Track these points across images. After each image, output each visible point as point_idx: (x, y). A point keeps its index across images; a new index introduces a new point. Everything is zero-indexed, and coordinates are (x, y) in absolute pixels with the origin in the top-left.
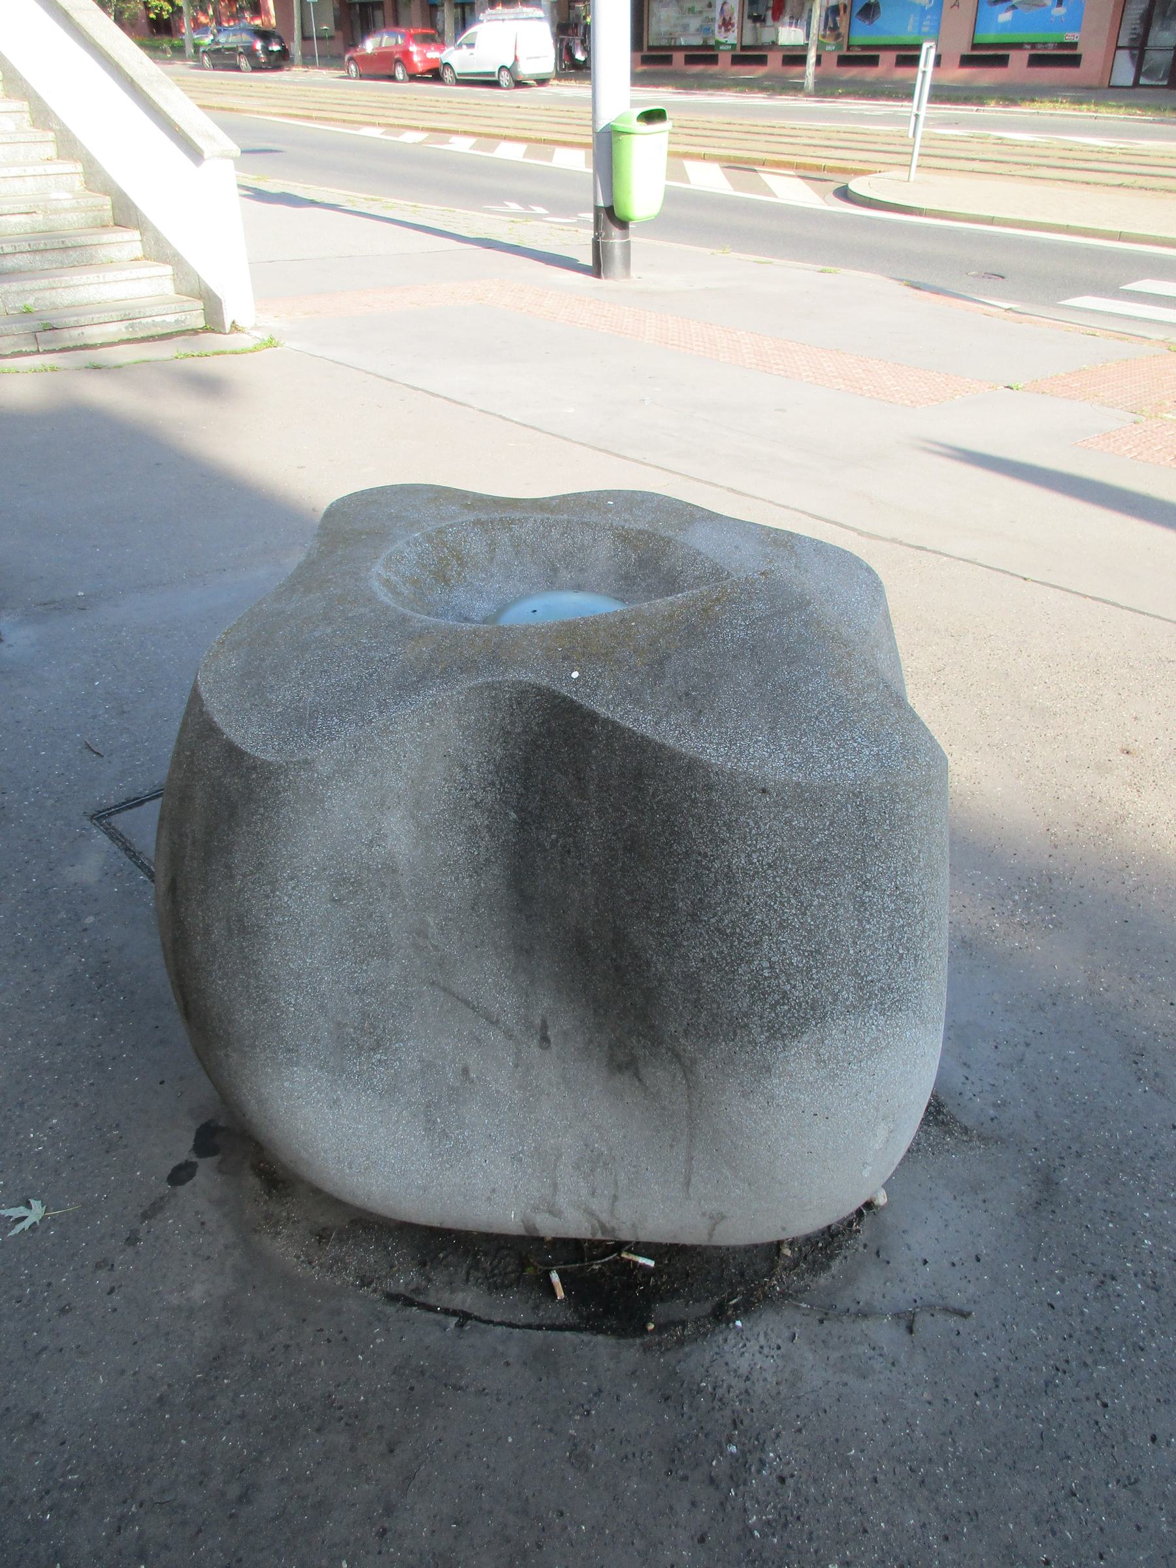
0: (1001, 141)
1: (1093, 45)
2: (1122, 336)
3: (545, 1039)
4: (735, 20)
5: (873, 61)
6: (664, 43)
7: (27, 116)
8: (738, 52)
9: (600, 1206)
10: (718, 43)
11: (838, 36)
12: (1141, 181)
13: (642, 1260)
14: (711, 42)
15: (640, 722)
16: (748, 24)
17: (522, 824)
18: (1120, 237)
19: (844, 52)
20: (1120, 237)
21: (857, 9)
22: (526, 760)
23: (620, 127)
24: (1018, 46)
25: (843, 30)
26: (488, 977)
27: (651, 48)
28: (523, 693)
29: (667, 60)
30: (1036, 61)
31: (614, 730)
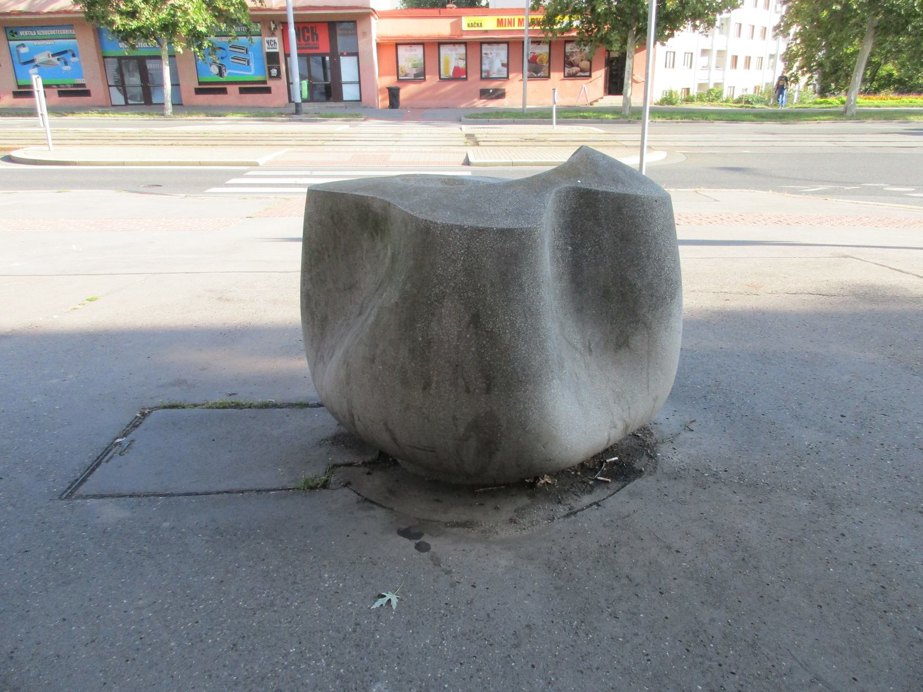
1: (95, 83)
2: (258, 198)
3: (591, 351)
12: (184, 142)
13: (613, 459)
17: (575, 251)
18: (200, 164)
22: (571, 221)
28: (568, 191)
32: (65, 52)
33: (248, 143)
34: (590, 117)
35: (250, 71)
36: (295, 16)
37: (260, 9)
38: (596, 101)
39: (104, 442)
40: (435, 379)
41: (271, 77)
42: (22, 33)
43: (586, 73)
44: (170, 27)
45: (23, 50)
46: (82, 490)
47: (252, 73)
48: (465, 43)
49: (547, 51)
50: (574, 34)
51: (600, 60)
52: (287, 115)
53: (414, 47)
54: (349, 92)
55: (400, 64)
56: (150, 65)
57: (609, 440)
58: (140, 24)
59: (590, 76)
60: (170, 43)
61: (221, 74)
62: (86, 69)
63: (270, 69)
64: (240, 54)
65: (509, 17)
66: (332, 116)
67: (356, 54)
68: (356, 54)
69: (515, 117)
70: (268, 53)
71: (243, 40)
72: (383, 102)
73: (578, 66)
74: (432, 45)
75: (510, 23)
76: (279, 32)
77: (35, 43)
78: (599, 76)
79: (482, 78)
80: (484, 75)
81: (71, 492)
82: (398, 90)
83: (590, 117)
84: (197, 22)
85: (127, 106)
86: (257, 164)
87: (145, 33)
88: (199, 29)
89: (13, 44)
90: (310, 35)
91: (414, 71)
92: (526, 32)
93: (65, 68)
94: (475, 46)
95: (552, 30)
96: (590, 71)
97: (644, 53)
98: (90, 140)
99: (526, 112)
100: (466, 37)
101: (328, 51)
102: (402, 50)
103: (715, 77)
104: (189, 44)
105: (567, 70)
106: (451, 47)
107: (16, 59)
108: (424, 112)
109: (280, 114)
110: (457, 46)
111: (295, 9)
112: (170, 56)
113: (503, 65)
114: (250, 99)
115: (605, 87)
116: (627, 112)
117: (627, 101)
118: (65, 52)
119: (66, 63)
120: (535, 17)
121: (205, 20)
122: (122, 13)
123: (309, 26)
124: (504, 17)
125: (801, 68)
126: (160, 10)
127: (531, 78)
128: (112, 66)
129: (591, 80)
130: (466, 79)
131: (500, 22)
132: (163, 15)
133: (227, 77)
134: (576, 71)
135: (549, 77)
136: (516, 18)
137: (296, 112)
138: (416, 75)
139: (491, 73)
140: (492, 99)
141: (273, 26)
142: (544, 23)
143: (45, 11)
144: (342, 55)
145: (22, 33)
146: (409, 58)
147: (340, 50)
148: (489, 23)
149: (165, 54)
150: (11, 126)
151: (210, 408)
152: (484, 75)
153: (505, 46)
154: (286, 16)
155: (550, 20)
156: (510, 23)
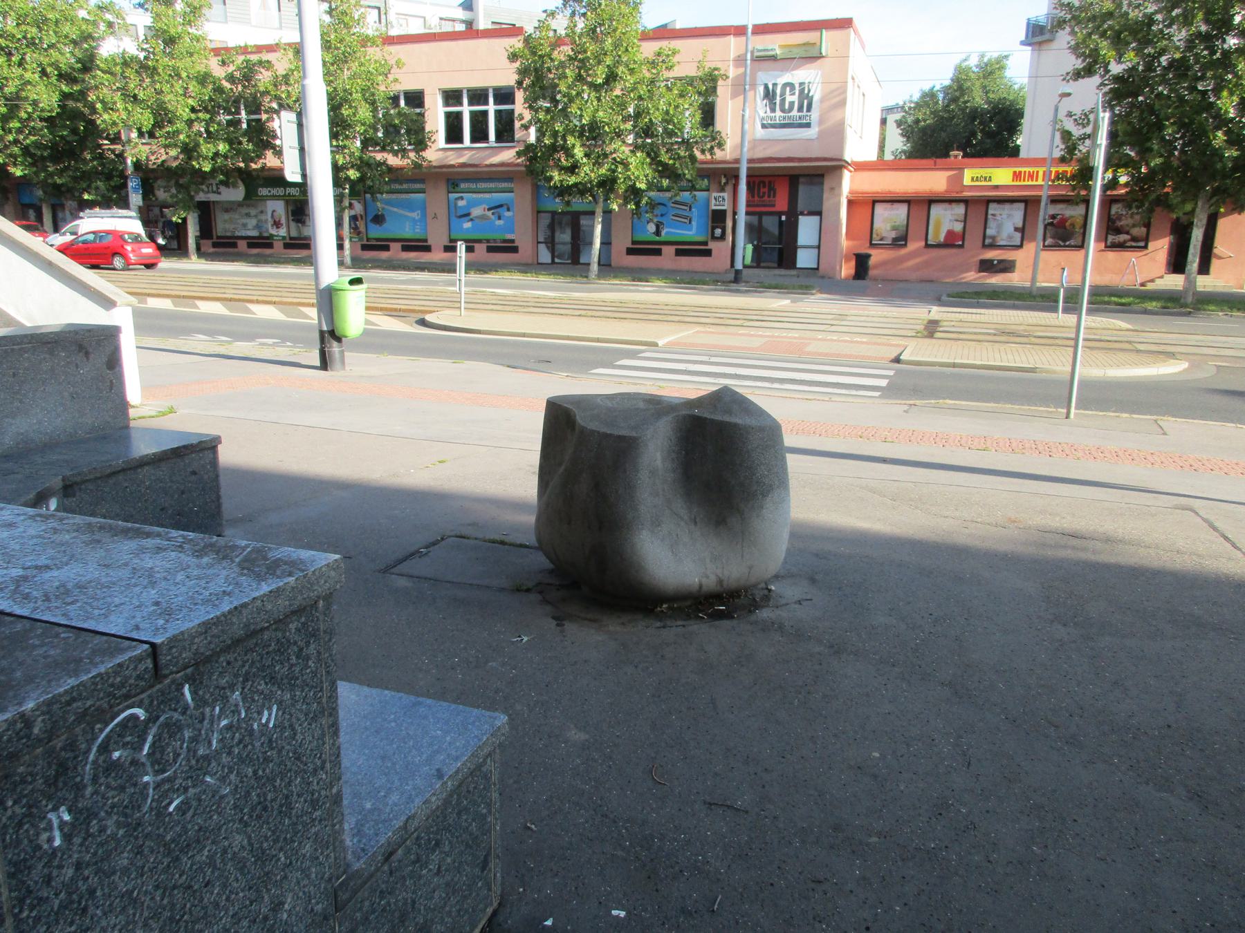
0: (495, 294)
1: (523, 236)
4: (283, 221)
5: (387, 248)
6: (229, 234)
7: (1028, 284)
8: (288, 241)
9: (719, 572)
10: (272, 236)
11: (359, 233)
12: (594, 313)
14: (266, 235)
15: (718, 417)
16: (293, 225)
18: (598, 340)
19: (365, 242)
20: (598, 340)
21: (370, 218)
23: (338, 286)
24: (479, 241)
25: (362, 229)
26: (680, 505)
27: (218, 237)
28: (684, 417)
29: (234, 245)
30: (491, 249)
31: (712, 421)
32: (501, 206)
33: (660, 317)
35: (690, 230)
36: (748, 169)
37: (712, 162)
38: (1152, 281)
39: (413, 549)
41: (714, 238)
42: (462, 186)
43: (1141, 243)
44: (608, 184)
45: (461, 203)
46: (395, 570)
47: (692, 232)
48: (966, 202)
52: (723, 282)
53: (896, 205)
54: (804, 259)
55: (875, 226)
56: (584, 221)
57: (701, 586)
58: (579, 180)
59: (1146, 247)
60: (606, 199)
61: (658, 233)
62: (519, 224)
63: (713, 228)
64: (684, 211)
65: (1031, 170)
66: (770, 287)
67: (819, 213)
68: (819, 213)
69: (1018, 299)
70: (714, 211)
71: (686, 195)
72: (846, 270)
73: (1127, 233)
74: (921, 204)
75: (1031, 176)
76: (729, 188)
77: (474, 196)
78: (1161, 247)
79: (927, 246)
80: (987, 241)
81: (386, 570)
82: (868, 256)
84: (638, 178)
85: (550, 268)
86: (656, 345)
87: (581, 189)
88: (638, 185)
89: (453, 196)
90: (766, 190)
91: (893, 235)
92: (1046, 188)
93: (501, 222)
94: (979, 205)
97: (1083, 252)
98: (504, 305)
100: (966, 194)
101: (785, 208)
102: (879, 209)
104: (626, 202)
105: (1110, 238)
106: (946, 205)
107: (452, 210)
108: (896, 289)
109: (716, 282)
110: (954, 205)
111: (750, 161)
112: (604, 212)
113: (1016, 229)
114: (686, 262)
116: (1190, 300)
118: (501, 206)
119: (499, 218)
121: (646, 176)
122: (561, 169)
123: (767, 180)
124: (1023, 170)
126: (600, 165)
127: (1046, 247)
128: (545, 220)
129: (1145, 252)
130: (962, 246)
131: (1017, 176)
132: (603, 171)
133: (663, 238)
137: (734, 280)
138: (895, 240)
141: (723, 181)
142: (1073, 177)
143: (488, 162)
144: (802, 214)
145: (462, 186)
146: (888, 219)
147: (800, 207)
149: (599, 211)
150: (435, 283)
152: (987, 241)
153: (1022, 206)
154: (738, 169)
156: (1031, 176)
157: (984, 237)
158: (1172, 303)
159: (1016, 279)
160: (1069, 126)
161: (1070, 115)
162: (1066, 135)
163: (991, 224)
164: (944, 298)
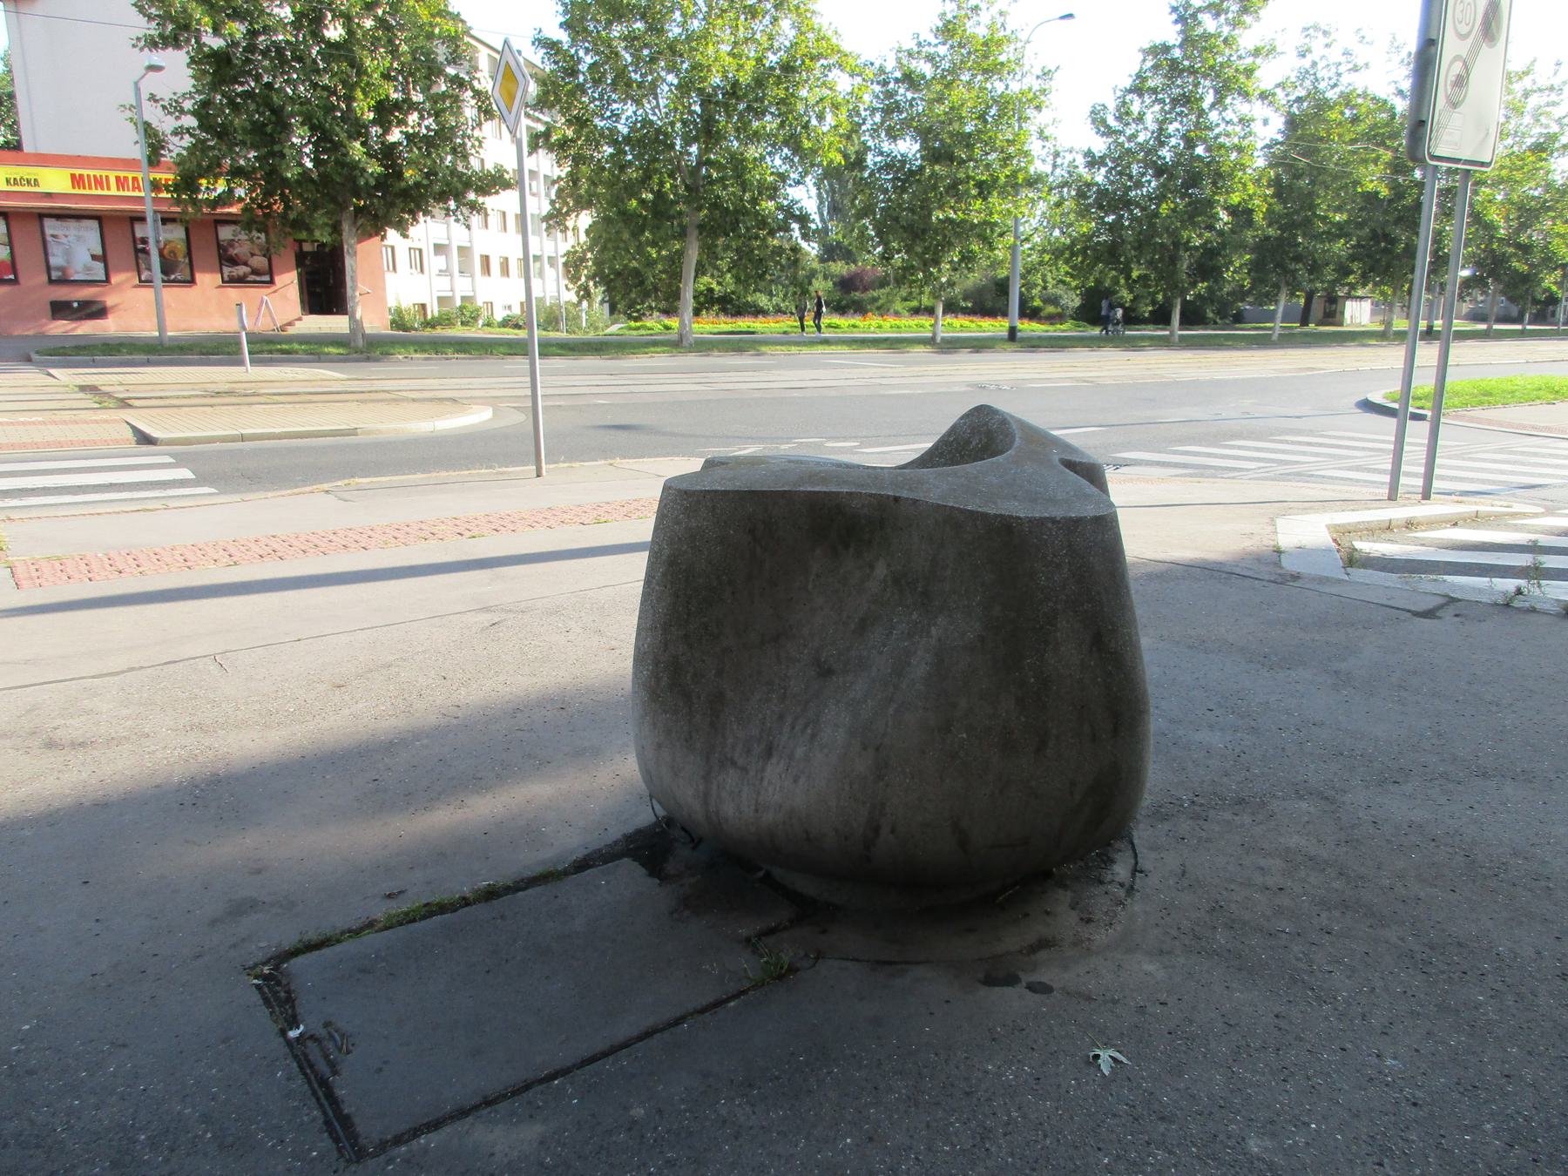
34: (296, 352)
40: (1054, 731)
43: (265, 277)
49: (183, 235)
50: (234, 210)
51: (287, 256)
59: (272, 282)
65: (98, 173)
73: (246, 264)
75: (99, 182)
78: (289, 282)
79: (51, 281)
83: (296, 352)
92: (149, 202)
95: (194, 202)
96: (271, 272)
99: (167, 344)
103: (462, 287)
105: (226, 270)
115: (302, 301)
116: (360, 343)
117: (356, 325)
120: (158, 176)
124: (85, 172)
125: (592, 277)
131: (77, 181)
134: (244, 273)
135: (192, 281)
136: (112, 176)
139: (71, 271)
140: (81, 319)
142: (177, 188)
148: (55, 181)
151: (386, 928)
152: (55, 275)
155: (187, 183)
156: (99, 182)
157: (48, 268)
158: (314, 350)
159: (108, 327)
160: (153, 115)
161: (153, 98)
162: (148, 130)
163: (53, 248)
164: (35, 357)
